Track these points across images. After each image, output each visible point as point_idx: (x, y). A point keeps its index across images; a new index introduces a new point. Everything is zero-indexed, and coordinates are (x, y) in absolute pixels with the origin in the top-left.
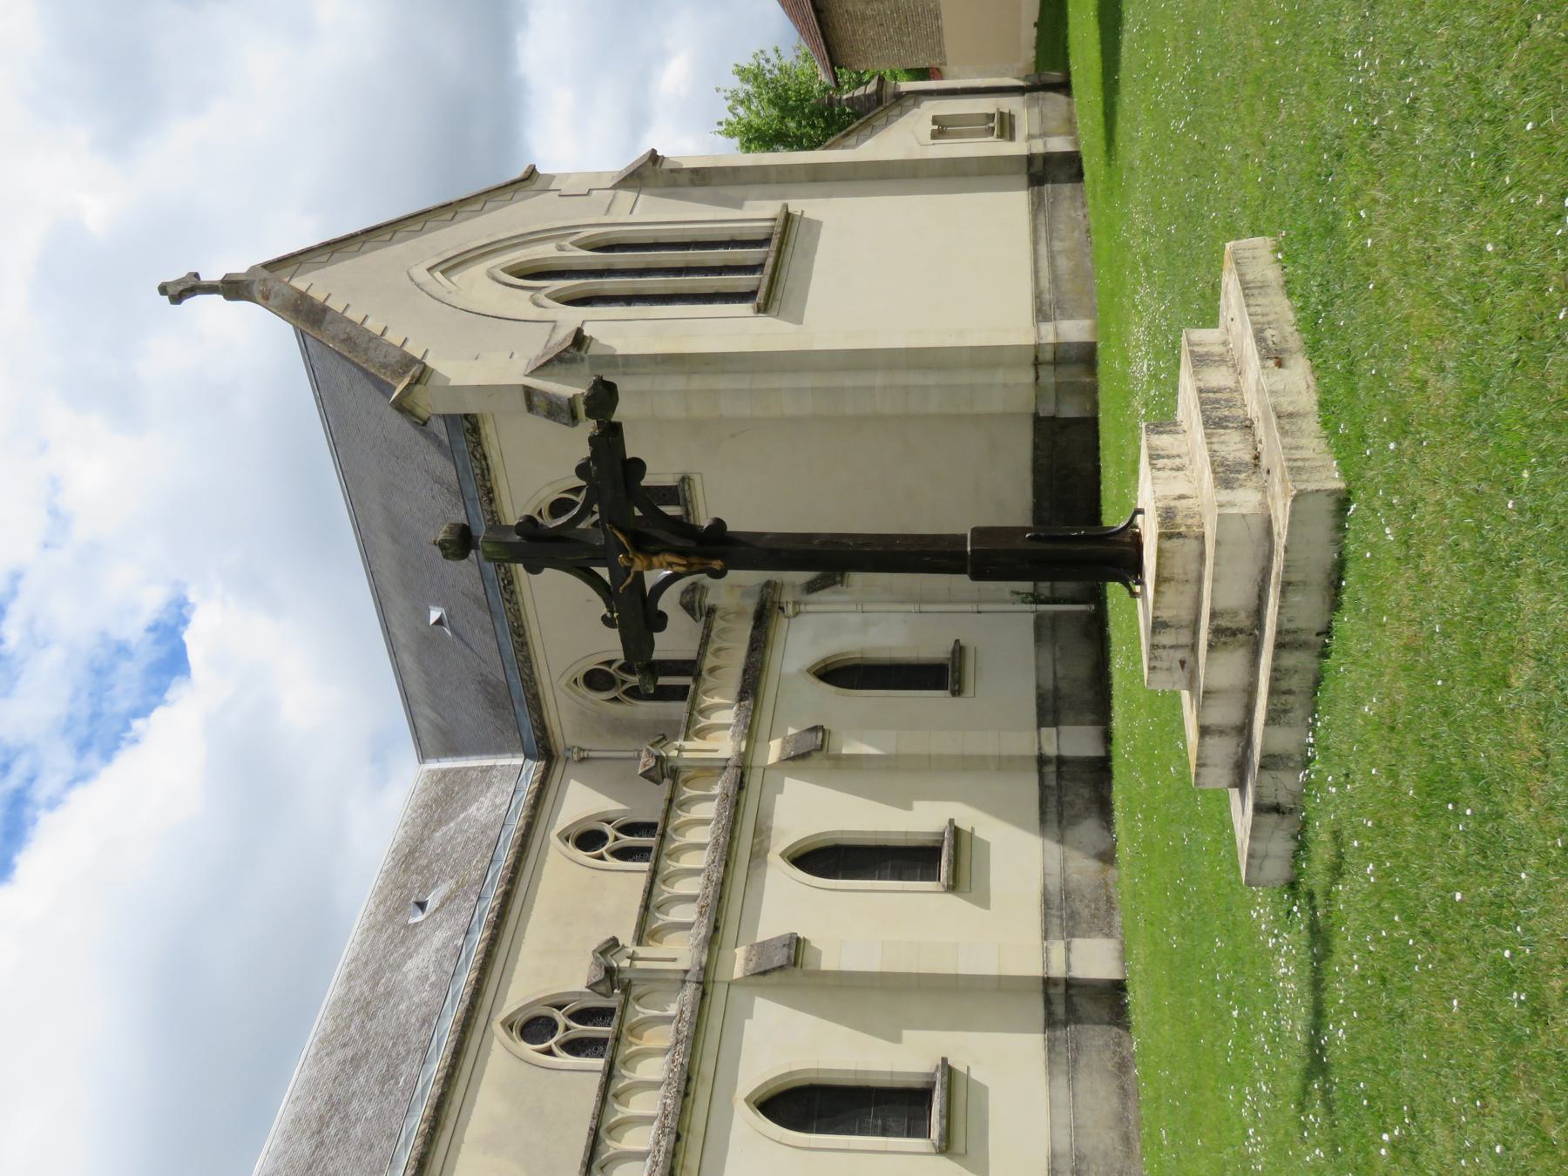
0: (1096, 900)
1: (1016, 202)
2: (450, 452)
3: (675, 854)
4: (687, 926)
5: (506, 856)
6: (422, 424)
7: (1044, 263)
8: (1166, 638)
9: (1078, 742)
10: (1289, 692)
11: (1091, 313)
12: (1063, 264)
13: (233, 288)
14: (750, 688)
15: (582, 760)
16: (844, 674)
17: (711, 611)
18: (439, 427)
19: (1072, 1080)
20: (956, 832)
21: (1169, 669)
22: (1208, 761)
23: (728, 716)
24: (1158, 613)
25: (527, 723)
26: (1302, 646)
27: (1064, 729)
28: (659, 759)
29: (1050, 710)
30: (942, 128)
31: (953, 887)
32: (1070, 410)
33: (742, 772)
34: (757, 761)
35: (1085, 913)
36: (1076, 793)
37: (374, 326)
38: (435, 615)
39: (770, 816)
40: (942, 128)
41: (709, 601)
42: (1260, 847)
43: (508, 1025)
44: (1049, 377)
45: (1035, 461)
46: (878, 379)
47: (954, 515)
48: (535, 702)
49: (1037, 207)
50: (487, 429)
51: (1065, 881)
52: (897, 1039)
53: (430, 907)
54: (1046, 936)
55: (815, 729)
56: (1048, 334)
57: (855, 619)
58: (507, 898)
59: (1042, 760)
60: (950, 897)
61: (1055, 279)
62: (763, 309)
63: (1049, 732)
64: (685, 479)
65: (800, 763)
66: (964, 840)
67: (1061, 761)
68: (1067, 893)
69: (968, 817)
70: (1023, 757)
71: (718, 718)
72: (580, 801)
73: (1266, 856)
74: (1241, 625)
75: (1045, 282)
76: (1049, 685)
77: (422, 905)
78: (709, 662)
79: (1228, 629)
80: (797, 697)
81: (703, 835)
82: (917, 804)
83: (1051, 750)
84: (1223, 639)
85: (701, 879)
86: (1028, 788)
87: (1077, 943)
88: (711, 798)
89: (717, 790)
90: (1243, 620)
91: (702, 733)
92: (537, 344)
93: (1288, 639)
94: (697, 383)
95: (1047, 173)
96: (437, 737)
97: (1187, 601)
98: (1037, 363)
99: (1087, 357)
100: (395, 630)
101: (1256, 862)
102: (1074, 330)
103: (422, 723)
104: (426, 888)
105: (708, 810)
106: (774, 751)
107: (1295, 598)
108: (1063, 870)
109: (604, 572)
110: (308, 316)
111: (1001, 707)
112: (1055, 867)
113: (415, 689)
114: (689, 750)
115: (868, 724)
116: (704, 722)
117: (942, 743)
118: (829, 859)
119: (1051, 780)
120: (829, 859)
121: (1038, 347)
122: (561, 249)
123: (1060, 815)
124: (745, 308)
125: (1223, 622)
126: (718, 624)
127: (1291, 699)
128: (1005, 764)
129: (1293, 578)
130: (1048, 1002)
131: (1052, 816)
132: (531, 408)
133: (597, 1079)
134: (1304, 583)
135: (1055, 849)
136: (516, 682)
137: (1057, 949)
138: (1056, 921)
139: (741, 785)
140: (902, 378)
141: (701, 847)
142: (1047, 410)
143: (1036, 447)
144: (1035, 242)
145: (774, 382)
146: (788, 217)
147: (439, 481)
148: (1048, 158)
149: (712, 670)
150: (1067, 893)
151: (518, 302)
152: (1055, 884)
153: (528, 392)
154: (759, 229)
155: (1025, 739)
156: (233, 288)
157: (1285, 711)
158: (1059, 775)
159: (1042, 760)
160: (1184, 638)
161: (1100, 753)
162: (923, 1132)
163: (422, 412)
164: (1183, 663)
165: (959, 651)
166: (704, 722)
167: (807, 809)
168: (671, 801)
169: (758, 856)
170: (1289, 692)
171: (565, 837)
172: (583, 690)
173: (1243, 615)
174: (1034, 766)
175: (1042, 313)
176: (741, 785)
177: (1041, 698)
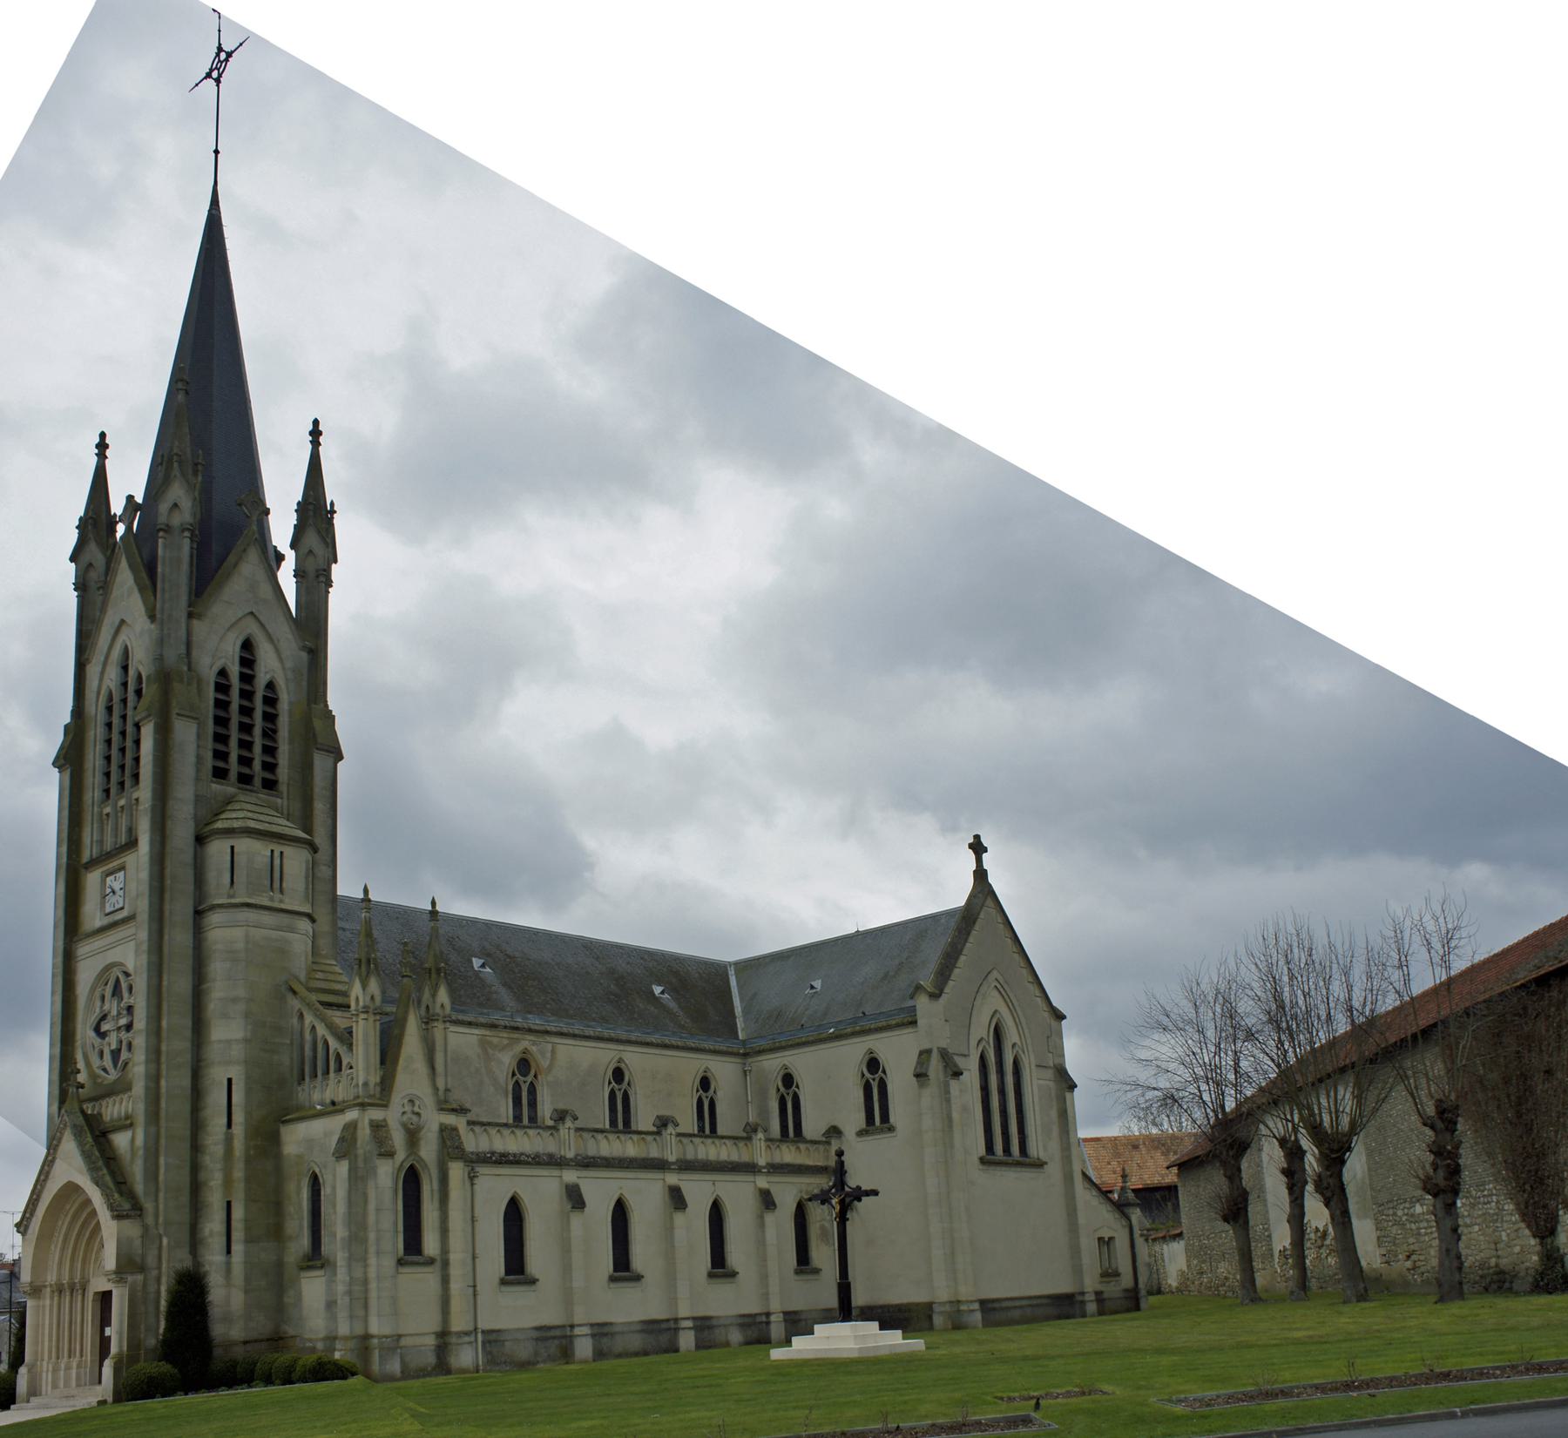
7: (1017, 1303)
13: (980, 875)
17: (829, 1143)
19: (642, 1331)
30: (1105, 1243)
40: (1105, 1243)
54: (592, 1325)
59: (768, 1314)
61: (1008, 1309)
62: (982, 1161)
63: (1093, 1297)
68: (710, 1328)
75: (1005, 1304)
78: (802, 1146)
83: (773, 1318)
87: (692, 1333)
115: (781, 1225)
122: (1014, 1045)
124: (982, 1151)
126: (821, 1147)
130: (563, 1327)
133: (600, 1126)
137: (586, 1330)
144: (1030, 1298)
151: (981, 1029)
154: (1034, 1149)
155: (776, 1305)
156: (980, 875)
159: (768, 1314)
162: (615, 1270)
167: (738, 1195)
177: (795, 1313)
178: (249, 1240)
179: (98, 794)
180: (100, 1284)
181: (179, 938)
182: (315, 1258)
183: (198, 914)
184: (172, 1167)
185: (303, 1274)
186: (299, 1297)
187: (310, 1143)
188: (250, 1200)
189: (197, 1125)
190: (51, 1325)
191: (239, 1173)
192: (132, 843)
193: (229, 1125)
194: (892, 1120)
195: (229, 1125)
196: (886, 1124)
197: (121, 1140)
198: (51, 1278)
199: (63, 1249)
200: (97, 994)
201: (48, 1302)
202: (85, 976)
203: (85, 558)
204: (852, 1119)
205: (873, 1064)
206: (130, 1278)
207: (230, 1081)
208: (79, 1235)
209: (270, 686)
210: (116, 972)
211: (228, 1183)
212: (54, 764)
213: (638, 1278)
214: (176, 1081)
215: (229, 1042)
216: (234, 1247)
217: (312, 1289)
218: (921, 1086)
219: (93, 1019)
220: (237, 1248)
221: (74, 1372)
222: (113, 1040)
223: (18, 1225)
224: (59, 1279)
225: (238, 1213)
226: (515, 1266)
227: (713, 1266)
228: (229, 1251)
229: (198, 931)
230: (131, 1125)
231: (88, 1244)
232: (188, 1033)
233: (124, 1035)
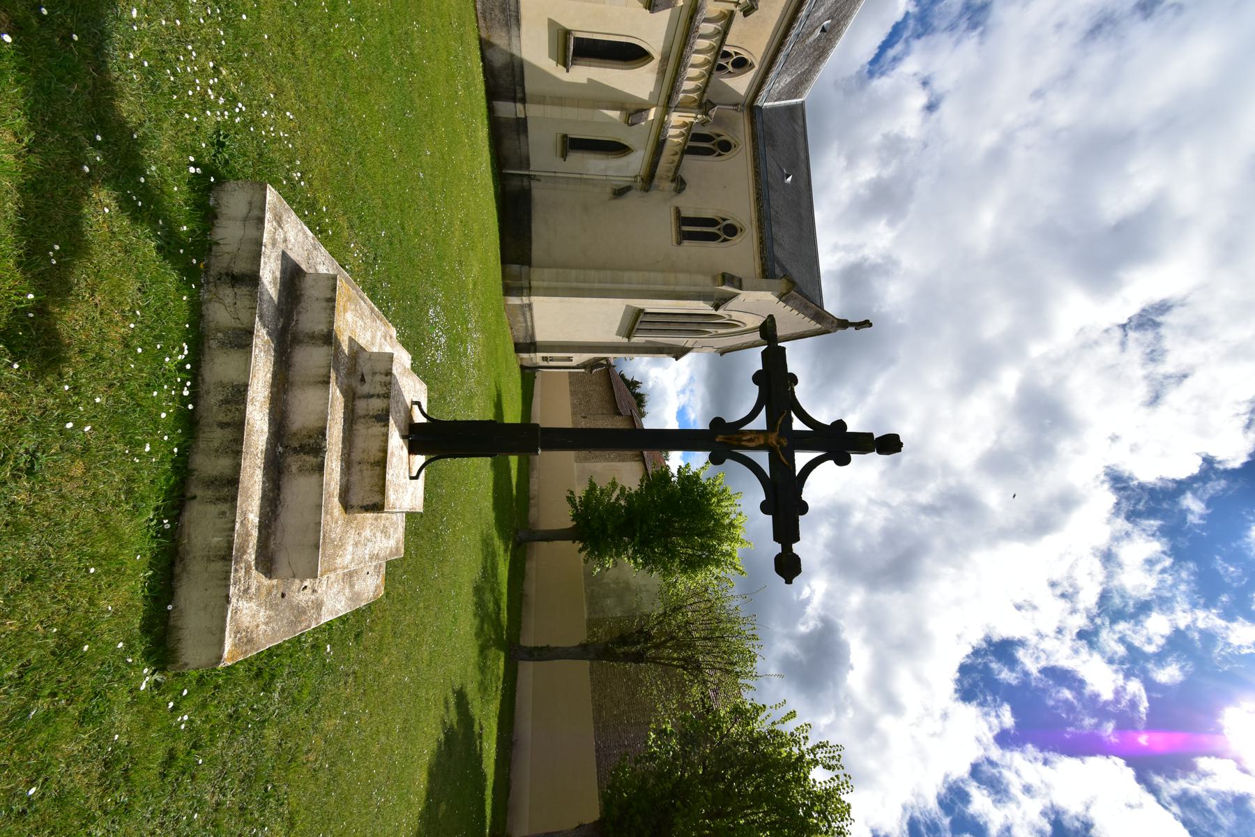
0: (492, 19)
1: (540, 337)
2: (775, 259)
3: (707, 62)
4: (707, 20)
5: (781, 58)
6: (786, 276)
8: (377, 404)
9: (506, 109)
10: (223, 425)
11: (506, 305)
12: (521, 319)
14: (660, 144)
15: (736, 105)
16: (617, 148)
17: (673, 181)
18: (778, 271)
20: (565, 65)
21: (374, 373)
22: (324, 304)
23: (672, 132)
24: (384, 430)
25: (759, 126)
26: (212, 482)
27: (513, 116)
28: (706, 114)
29: (521, 125)
30: (569, 359)
31: (567, 33)
32: (515, 268)
33: (668, 103)
34: (660, 109)
35: (497, 12)
36: (505, 80)
37: (795, 312)
38: (789, 179)
39: (657, 80)
41: (673, 185)
42: (251, 232)
43: (752, 66)
44: (525, 283)
45: (530, 243)
46: (596, 285)
47: (544, 546)
48: (754, 137)
49: (533, 335)
50: (758, 271)
51: (509, 32)
52: (589, 80)
53: (819, 29)
55: (632, 125)
56: (525, 300)
57: (610, 173)
58: (785, 35)
60: (569, 27)
61: (524, 314)
64: (679, 243)
65: (639, 107)
66: (561, 60)
67: (514, 100)
68: (507, 25)
69: (559, 72)
70: (533, 103)
71: (677, 131)
72: (741, 84)
73: (245, 219)
74: (295, 457)
76: (522, 137)
77: (823, 30)
79: (308, 453)
80: (639, 140)
81: (692, 72)
82: (585, 81)
83: (519, 106)
84: (312, 441)
85: (695, 47)
86: (530, 86)
88: (685, 91)
89: (681, 96)
90: (294, 463)
91: (685, 124)
92: (732, 304)
93: (225, 491)
94: (671, 288)
95: (532, 346)
96: (795, 115)
97: (360, 443)
98: (530, 288)
99: (508, 291)
100: (805, 175)
101: (255, 213)
102: (514, 301)
103: (800, 123)
104: (819, 39)
105: (687, 85)
106: (652, 114)
107: (217, 540)
108: (510, 39)
109: (797, 425)
110: (819, 315)
111: (544, 125)
112: (514, 40)
113: (801, 140)
114: (689, 117)
116: (683, 130)
117: (571, 113)
118: (629, 54)
119: (518, 89)
120: (629, 54)
121: (529, 295)
123: (513, 70)
125: (311, 460)
126: (670, 174)
127: (221, 417)
128: (542, 100)
129: (219, 566)
131: (517, 69)
132: (740, 280)
134: (209, 560)
135: (515, 52)
136: (761, 148)
138: (512, 8)
139: (669, 98)
140: (586, 285)
141: (693, 66)
142: (525, 268)
143: (530, 250)
145: (639, 287)
146: (629, 337)
147: (780, 245)
148: (529, 352)
149: (676, 154)
150: (507, 25)
151: (735, 315)
152: (514, 32)
153: (740, 288)
155: (533, 111)
157: (226, 401)
158: (515, 91)
160: (361, 406)
161: (495, 103)
162: (576, 39)
163: (784, 281)
164: (363, 380)
165: (564, 156)
166: (683, 130)
167: (638, 82)
168: (704, 92)
169: (665, 58)
170: (223, 425)
171: (752, 66)
172: (732, 142)
173: (294, 468)
174: (528, 98)
175: (530, 306)
176: (669, 98)
177: (526, 131)
194: (686, 243)
196: (684, 236)
204: (692, 205)
205: (731, 231)
213: (679, 243)
218: (714, 278)
226: (573, 145)
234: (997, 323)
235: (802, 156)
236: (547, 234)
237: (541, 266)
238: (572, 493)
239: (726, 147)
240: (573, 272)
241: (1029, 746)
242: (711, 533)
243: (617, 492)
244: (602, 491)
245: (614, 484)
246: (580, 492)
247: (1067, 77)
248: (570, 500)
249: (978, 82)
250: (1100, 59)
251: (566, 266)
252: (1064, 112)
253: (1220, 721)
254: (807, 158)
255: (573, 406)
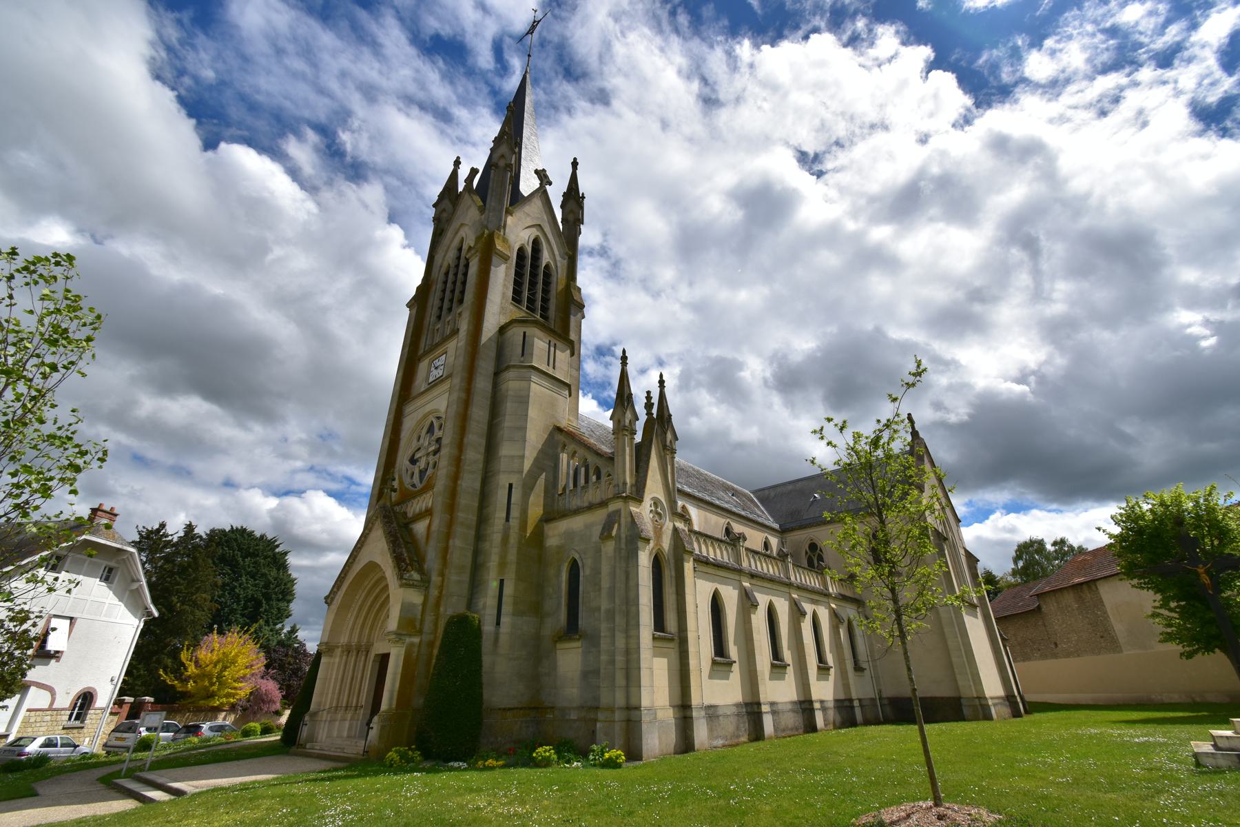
103: (767, 492)
178: (517, 613)
179: (433, 318)
180: (379, 648)
181: (483, 384)
182: (572, 629)
183: (497, 374)
184: (460, 545)
185: (559, 646)
186: (554, 667)
187: (569, 535)
188: (519, 578)
189: (482, 519)
190: (336, 679)
191: (512, 556)
192: (455, 332)
193: (507, 519)
195: (507, 519)
197: (420, 527)
198: (344, 640)
199: (357, 617)
200: (415, 436)
201: (337, 660)
202: (408, 424)
203: (443, 206)
206: (408, 640)
207: (511, 486)
208: (371, 606)
209: (547, 267)
210: (432, 418)
211: (502, 565)
212: (408, 305)
214: (470, 482)
215: (513, 457)
216: (504, 619)
217: (570, 660)
219: (410, 453)
220: (505, 619)
221: (347, 724)
222: (422, 464)
223: (326, 598)
224: (349, 642)
225: (509, 590)
227: (716, 655)
228: (498, 623)
229: (496, 386)
230: (431, 514)
231: (376, 616)
232: (482, 449)
233: (431, 459)
234: (829, 259)
235: (790, 487)
236: (930, 683)
237: (957, 688)
238: (1182, 654)
239: (813, 547)
240: (954, 659)
241: (1217, 650)
242: (1179, 520)
243: (1162, 611)
244: (1170, 625)
245: (1154, 615)
246: (1175, 648)
247: (645, 284)
248: (1190, 655)
249: (647, 338)
250: (634, 268)
251: (950, 666)
252: (667, 274)
253: (1214, 107)
254: (790, 483)
255: (1044, 657)
